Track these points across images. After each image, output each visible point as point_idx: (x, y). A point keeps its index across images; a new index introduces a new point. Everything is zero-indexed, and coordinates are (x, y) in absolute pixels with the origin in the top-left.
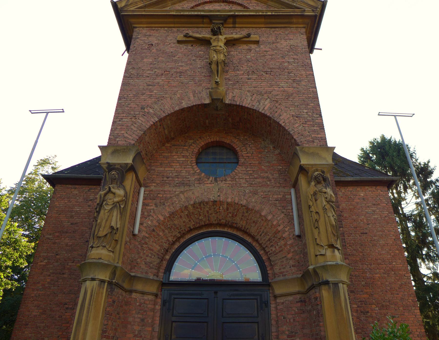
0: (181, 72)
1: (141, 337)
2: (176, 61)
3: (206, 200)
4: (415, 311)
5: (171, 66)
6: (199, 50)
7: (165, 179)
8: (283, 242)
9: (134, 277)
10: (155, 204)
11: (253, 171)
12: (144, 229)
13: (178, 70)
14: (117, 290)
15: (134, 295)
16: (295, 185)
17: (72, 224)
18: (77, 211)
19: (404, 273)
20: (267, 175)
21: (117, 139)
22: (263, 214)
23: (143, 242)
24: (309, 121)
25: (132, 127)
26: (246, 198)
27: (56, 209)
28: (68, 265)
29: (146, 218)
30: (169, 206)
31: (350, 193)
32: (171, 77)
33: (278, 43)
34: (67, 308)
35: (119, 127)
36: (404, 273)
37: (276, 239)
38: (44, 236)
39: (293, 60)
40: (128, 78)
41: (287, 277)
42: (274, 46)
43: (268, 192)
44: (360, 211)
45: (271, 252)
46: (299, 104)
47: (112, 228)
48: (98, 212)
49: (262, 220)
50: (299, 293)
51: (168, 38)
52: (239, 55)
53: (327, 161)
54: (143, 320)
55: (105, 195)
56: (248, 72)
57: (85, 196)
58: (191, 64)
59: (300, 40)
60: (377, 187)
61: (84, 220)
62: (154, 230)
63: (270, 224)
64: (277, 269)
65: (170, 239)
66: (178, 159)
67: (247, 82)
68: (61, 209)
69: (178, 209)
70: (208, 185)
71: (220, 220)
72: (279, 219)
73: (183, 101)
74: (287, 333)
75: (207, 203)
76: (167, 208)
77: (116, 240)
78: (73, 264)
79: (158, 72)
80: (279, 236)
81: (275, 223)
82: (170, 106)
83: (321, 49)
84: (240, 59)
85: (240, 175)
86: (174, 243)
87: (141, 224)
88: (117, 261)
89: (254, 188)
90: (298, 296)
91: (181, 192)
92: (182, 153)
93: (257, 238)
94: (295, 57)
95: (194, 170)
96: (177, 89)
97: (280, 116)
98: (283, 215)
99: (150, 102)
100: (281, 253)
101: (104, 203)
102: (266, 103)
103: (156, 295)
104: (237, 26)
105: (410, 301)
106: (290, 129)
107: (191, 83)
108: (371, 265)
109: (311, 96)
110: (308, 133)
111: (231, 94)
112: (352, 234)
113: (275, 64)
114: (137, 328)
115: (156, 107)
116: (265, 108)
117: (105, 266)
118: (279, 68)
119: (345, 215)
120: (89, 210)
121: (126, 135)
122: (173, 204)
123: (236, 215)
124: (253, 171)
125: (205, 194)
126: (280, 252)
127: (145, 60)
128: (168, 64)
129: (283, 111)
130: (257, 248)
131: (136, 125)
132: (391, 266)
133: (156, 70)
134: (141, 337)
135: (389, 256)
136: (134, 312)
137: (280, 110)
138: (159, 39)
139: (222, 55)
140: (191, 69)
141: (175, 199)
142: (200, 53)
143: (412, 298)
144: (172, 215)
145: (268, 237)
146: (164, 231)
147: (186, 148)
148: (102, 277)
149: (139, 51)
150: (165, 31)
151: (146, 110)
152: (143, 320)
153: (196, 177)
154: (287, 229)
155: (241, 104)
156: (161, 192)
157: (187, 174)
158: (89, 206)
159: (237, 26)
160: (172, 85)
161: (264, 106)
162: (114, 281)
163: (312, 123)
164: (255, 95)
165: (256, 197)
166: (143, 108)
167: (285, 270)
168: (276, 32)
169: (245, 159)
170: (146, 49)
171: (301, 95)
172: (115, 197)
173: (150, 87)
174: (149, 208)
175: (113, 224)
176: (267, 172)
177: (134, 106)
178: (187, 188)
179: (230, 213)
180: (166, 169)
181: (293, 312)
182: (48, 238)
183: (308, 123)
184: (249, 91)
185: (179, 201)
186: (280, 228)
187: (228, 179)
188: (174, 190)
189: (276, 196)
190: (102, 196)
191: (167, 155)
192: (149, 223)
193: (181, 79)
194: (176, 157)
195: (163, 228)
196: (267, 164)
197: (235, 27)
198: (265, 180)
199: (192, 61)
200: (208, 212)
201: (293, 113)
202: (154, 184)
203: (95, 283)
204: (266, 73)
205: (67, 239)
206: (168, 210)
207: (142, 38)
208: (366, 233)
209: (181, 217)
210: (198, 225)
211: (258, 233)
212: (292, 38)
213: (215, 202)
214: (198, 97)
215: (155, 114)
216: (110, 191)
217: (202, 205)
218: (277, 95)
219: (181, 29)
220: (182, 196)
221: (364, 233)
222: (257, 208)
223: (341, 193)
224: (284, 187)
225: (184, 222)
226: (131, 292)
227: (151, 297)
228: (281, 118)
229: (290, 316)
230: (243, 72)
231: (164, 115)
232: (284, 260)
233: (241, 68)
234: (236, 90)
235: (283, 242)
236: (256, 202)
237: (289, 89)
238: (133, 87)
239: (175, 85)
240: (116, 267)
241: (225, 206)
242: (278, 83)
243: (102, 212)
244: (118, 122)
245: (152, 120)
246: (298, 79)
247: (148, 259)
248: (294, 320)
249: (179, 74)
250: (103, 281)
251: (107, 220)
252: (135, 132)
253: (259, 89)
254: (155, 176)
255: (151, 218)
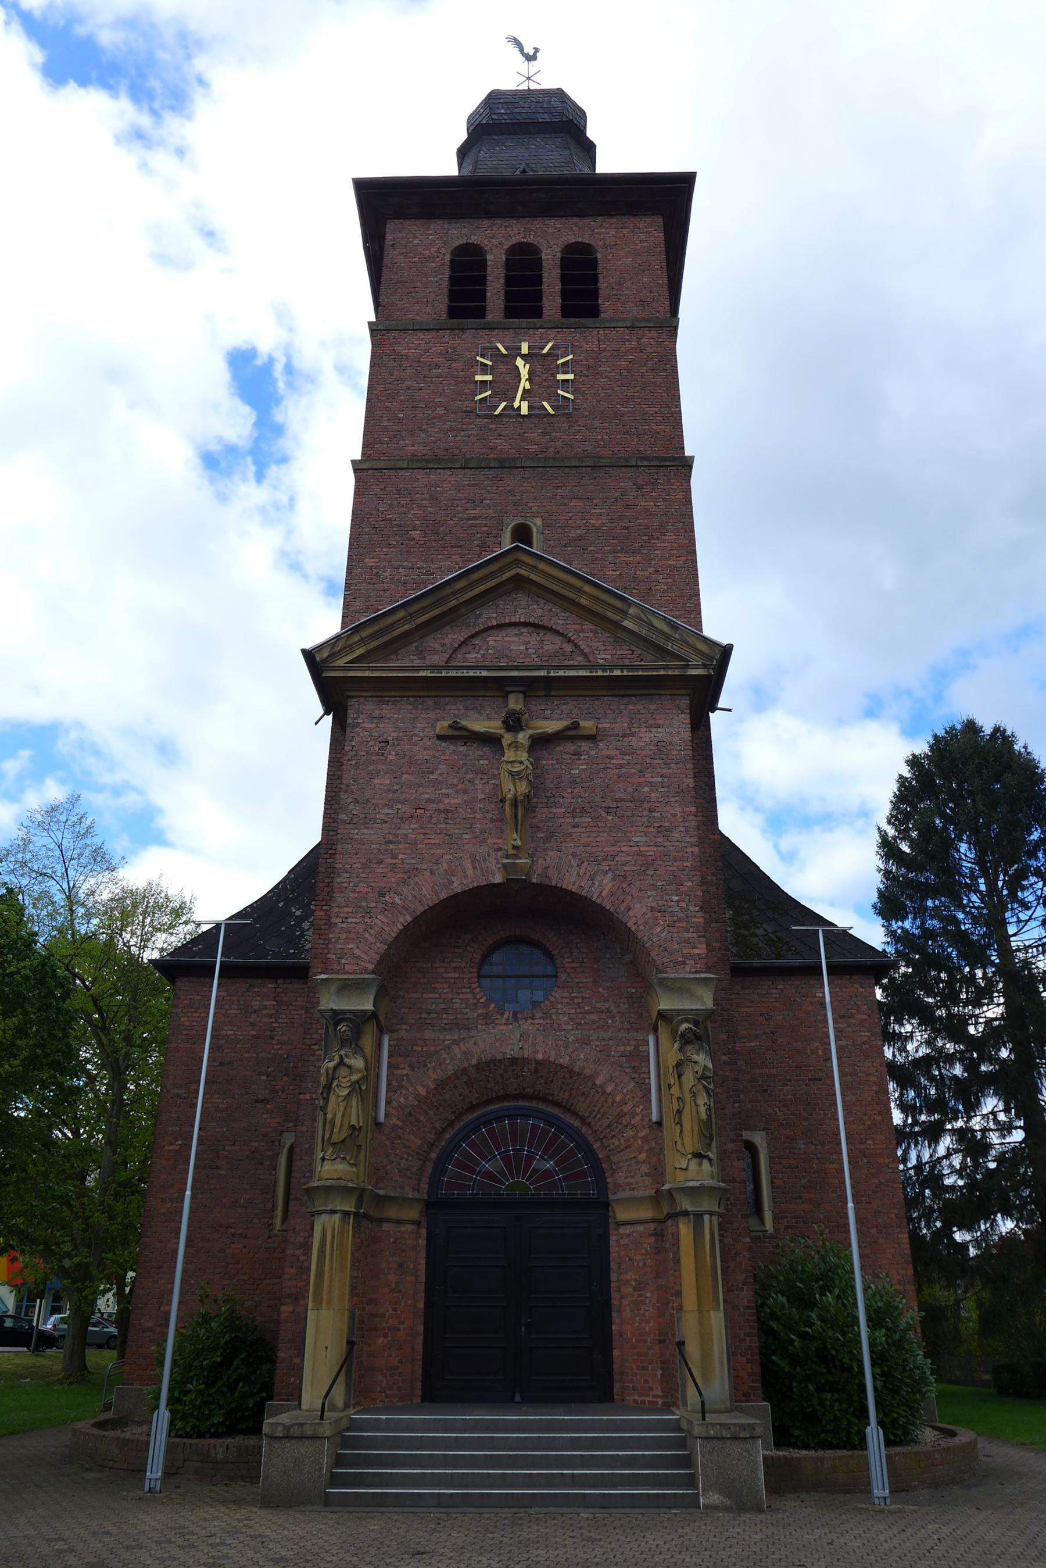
0: (448, 811)
1: (400, 1291)
2: (436, 783)
3: (499, 1057)
4: (900, 1236)
5: (427, 796)
6: (477, 755)
7: (424, 1015)
8: (630, 1133)
9: (385, 1197)
10: (410, 1066)
11: (583, 998)
12: (394, 1112)
13: (441, 806)
14: (366, 1223)
15: (385, 1226)
16: (655, 1030)
17: (221, 1064)
18: (228, 1036)
19: (887, 1161)
20: (607, 1005)
21: (343, 961)
22: (598, 1082)
23: (393, 1135)
24: (680, 920)
25: (367, 935)
26: (569, 1051)
27: (185, 1032)
28: (224, 1150)
29: (396, 1092)
30: (434, 1068)
31: (793, 991)
32: (429, 822)
33: (633, 735)
34: (233, 1235)
35: (343, 936)
36: (887, 1161)
37: (620, 1127)
38: (168, 1091)
39: (660, 780)
40: (348, 826)
41: (636, 1193)
42: (626, 744)
43: (610, 1039)
44: (812, 1030)
45: (612, 1147)
46: (664, 883)
47: (353, 1127)
48: (326, 1100)
49: (597, 1092)
50: (653, 1221)
51: (418, 725)
52: (556, 766)
53: (704, 1004)
54: (401, 1265)
55: (335, 1068)
56: (574, 811)
57: (242, 1002)
58: (465, 792)
59: (676, 727)
60: (854, 977)
61: (246, 1055)
62: (410, 1114)
63: (610, 1100)
64: (621, 1177)
65: (438, 1125)
66: (445, 975)
67: (570, 834)
68: (194, 1032)
69: (450, 1073)
70: (502, 1027)
71: (524, 1089)
72: (625, 1090)
73: (454, 879)
74: (633, 1283)
75: (500, 1061)
76: (431, 1072)
77: (359, 1146)
78: (234, 1148)
79: (404, 810)
80: (625, 1120)
81: (618, 1099)
82: (429, 890)
83: (730, 710)
84: (560, 777)
85: (560, 1006)
86: (444, 1131)
87: (388, 1103)
88: (362, 1179)
89: (584, 1033)
90: (652, 1226)
91: (454, 1042)
92: (452, 961)
93: (589, 1120)
94: (665, 771)
95: (475, 998)
96: (441, 851)
97: (630, 909)
98: (632, 1084)
99: (393, 880)
100: (629, 1150)
101: (335, 1083)
102: (605, 881)
103: (418, 1223)
104: (553, 693)
105: (893, 1216)
106: (645, 938)
107: (467, 836)
108: (823, 1144)
109: (689, 864)
110: (676, 946)
111: (541, 861)
112: (790, 1081)
113: (625, 790)
114: (392, 1278)
115: (405, 891)
116: (604, 894)
117: (346, 1191)
118: (633, 800)
119: (780, 1040)
120: (254, 1033)
121: (357, 952)
122: (440, 1064)
123: (551, 1082)
124: (583, 998)
125: (497, 1044)
126: (626, 1148)
127: (376, 781)
128: (420, 790)
129: (635, 900)
130: (589, 1138)
131: (372, 932)
132: (863, 1147)
133: (399, 806)
134: (400, 1291)
135: (862, 1127)
136: (387, 1253)
137: (629, 897)
138: (400, 728)
139: (524, 783)
140: (465, 801)
141: (445, 1056)
142: (481, 762)
143: (896, 1211)
144: (441, 1085)
145: (608, 1121)
146: (426, 1113)
147: (460, 950)
148: (346, 1209)
149: (364, 758)
150: (410, 707)
151: (387, 898)
152: (401, 1265)
153: (479, 1011)
154: (638, 1110)
155: (559, 885)
156: (420, 1043)
157: (464, 1005)
158: (253, 1024)
159: (553, 693)
160: (433, 841)
161: (600, 888)
162: (362, 1211)
163: (684, 924)
164: (586, 863)
165: (588, 1049)
166: (382, 895)
167: (633, 1180)
168: (630, 707)
169: (569, 974)
170: (377, 754)
171: (670, 863)
172: (351, 1074)
173: (392, 846)
174: (399, 1072)
175: (354, 1122)
176: (608, 1001)
177: (366, 889)
178: (464, 1034)
179: (542, 1077)
180: (425, 996)
181: (643, 1251)
182: (178, 1096)
183: (677, 925)
184: (574, 855)
185: (452, 1059)
186: (626, 1109)
187: (538, 1016)
188: (441, 1037)
189: (622, 1048)
190: (331, 1072)
191: (424, 965)
192: (402, 1100)
193: (449, 826)
194: (442, 970)
195: (425, 1107)
196: (609, 984)
197: (550, 696)
198: (603, 1016)
199: (466, 783)
200: (502, 1076)
201: (654, 904)
202: (404, 1027)
203: (337, 1217)
204: (608, 810)
205: (216, 1096)
206: (434, 1076)
207: (365, 725)
208: (820, 1079)
209: (455, 1087)
210: (485, 1098)
211: (590, 1113)
212: (661, 722)
213: (514, 1061)
214: (481, 869)
215: (404, 907)
216: (342, 1062)
217: (492, 1066)
218: (626, 863)
219: (442, 699)
220: (456, 1049)
221: (815, 1079)
222: (589, 1071)
223: (775, 991)
224: (637, 1030)
225: (461, 1095)
226: (380, 1221)
227: (410, 1227)
228: (631, 913)
229: (639, 1258)
230: (563, 810)
231: (422, 909)
232: (633, 1162)
233: (561, 800)
234: (551, 853)
235: (630, 1133)
236: (586, 1060)
237: (648, 849)
238: (359, 846)
239: (437, 841)
240: (363, 1190)
241: (533, 1066)
242: (629, 834)
243: (332, 1099)
244: (340, 925)
245: (401, 920)
246: (667, 824)
247: (403, 1164)
248: (644, 1264)
249: (443, 815)
250: (346, 1214)
251: (343, 1115)
252: (372, 946)
253: (594, 850)
254: (406, 1010)
255: (404, 1092)
